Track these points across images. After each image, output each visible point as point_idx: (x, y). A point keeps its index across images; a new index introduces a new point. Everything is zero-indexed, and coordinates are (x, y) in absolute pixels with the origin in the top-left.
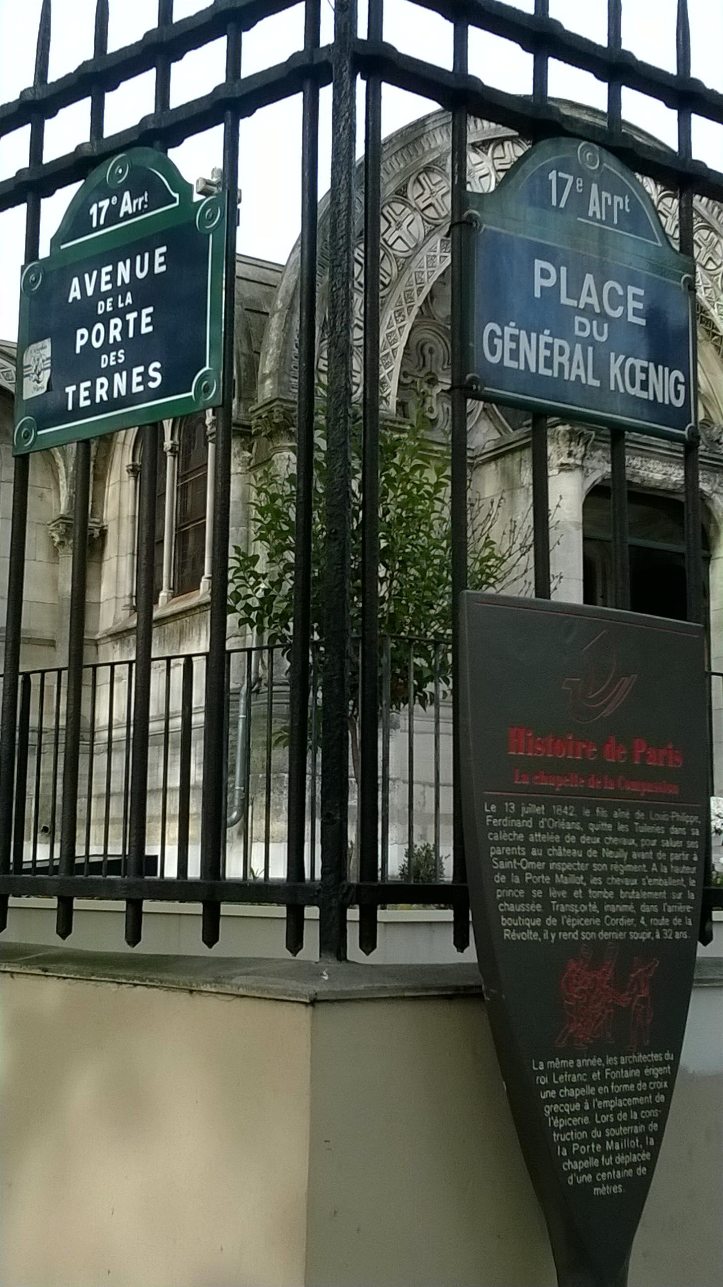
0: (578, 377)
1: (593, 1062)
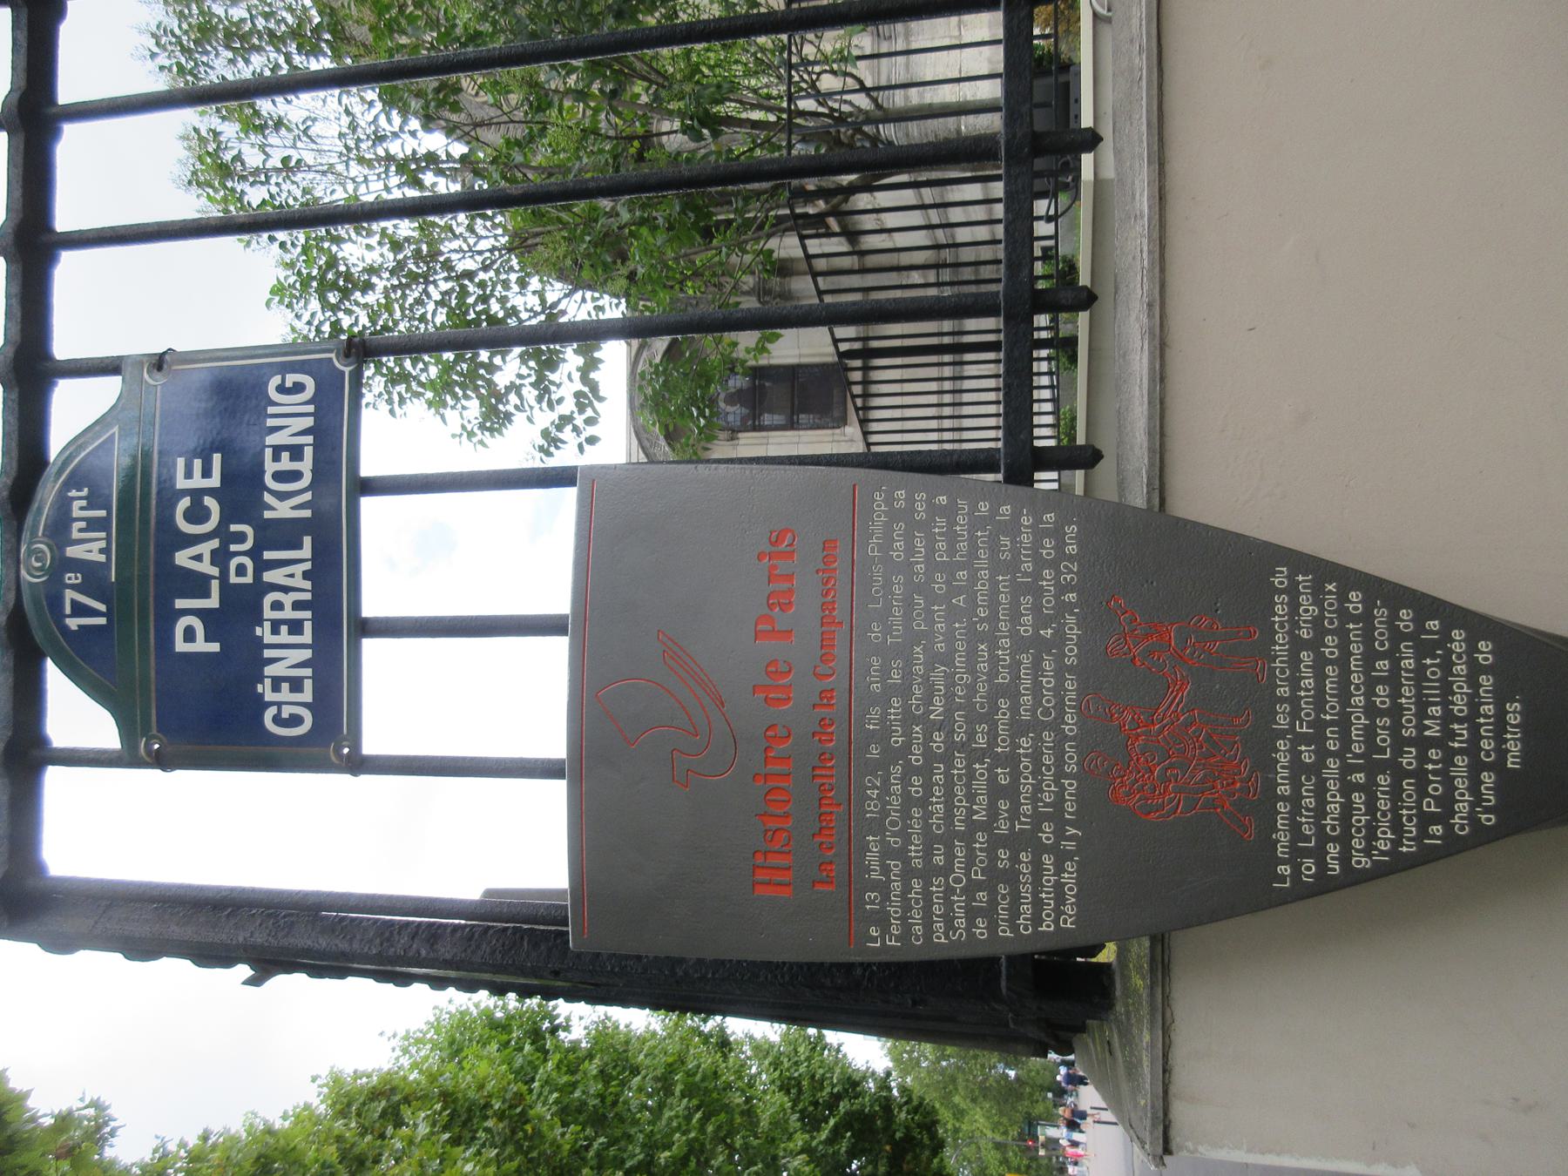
0: (306, 575)
1: (1283, 759)
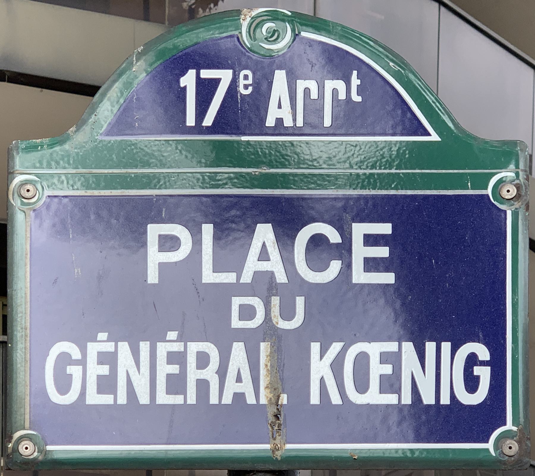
0: (239, 397)
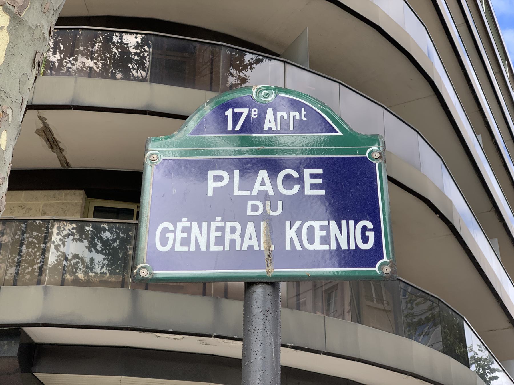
0: (251, 247)
